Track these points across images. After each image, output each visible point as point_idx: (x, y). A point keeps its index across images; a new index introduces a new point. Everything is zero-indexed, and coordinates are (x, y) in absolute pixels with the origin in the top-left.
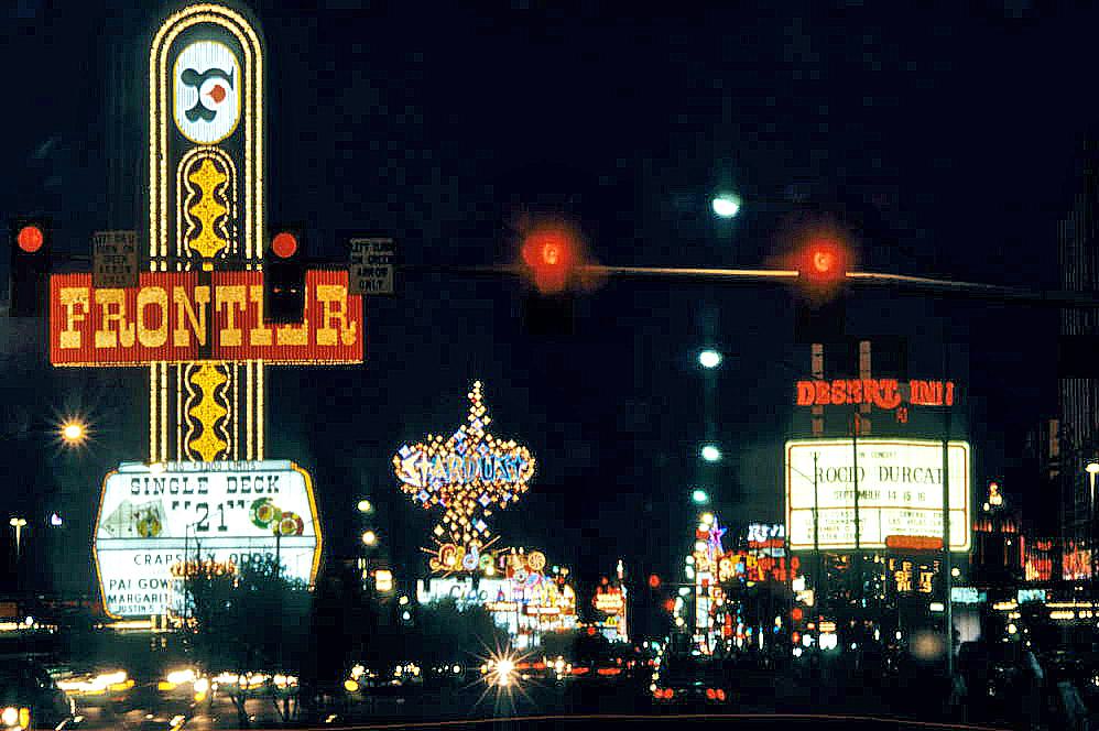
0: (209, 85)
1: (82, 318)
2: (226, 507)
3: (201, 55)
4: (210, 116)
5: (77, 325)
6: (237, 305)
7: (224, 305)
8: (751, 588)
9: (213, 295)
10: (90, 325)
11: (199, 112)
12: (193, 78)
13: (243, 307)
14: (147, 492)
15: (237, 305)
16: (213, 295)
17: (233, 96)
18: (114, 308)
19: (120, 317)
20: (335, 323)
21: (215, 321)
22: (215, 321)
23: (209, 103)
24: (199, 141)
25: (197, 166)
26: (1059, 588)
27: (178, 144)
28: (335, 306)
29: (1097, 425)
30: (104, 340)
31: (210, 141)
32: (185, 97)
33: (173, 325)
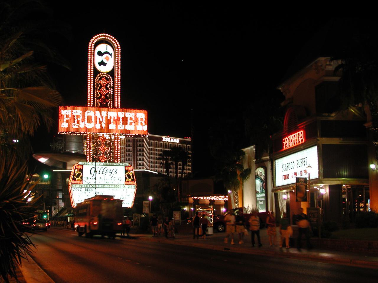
0: (105, 56)
1: (68, 119)
2: (292, 162)
3: (102, 48)
4: (105, 64)
5: (67, 121)
6: (114, 117)
7: (111, 117)
8: (240, 244)
9: (107, 114)
10: (71, 120)
11: (102, 63)
12: (100, 54)
13: (116, 118)
14: (305, 165)
15: (114, 117)
16: (107, 114)
17: (111, 59)
18: (78, 116)
19: (80, 119)
20: (142, 124)
21: (108, 122)
22: (108, 122)
23: (105, 61)
24: (102, 71)
25: (101, 79)
26: (14, 99)
27: (96, 72)
28: (142, 119)
29: (8, 224)
30: (75, 126)
31: (105, 72)
32: (98, 59)
33: (96, 122)
